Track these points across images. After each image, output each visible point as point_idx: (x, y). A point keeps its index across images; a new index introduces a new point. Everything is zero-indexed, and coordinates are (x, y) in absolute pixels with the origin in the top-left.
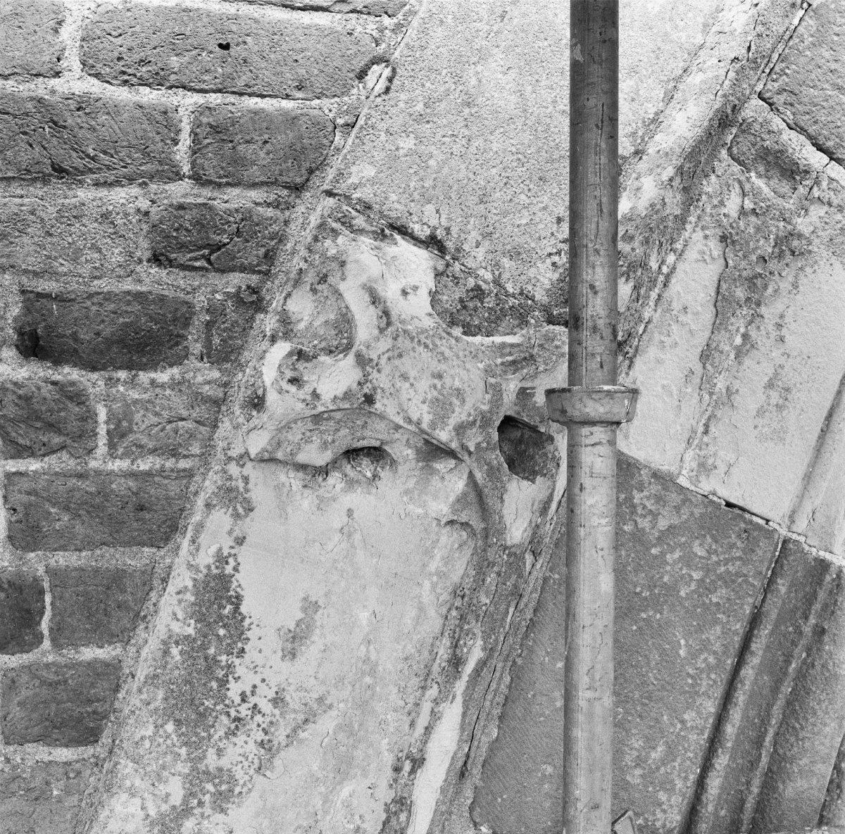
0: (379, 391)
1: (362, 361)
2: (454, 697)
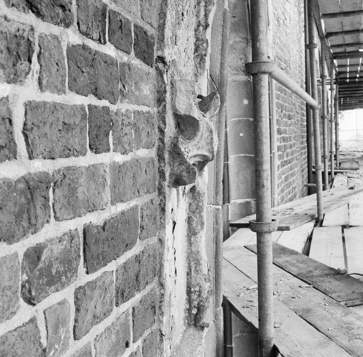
2: (214, 4)
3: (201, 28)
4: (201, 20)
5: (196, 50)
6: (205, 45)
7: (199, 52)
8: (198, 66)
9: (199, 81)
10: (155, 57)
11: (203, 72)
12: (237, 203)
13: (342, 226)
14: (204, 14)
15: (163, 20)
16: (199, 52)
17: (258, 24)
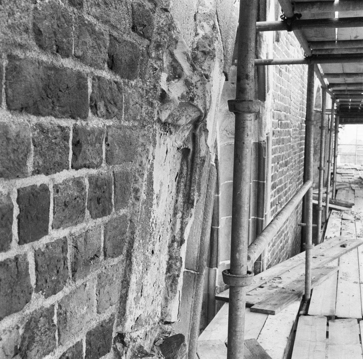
0: (197, 96)
1: (187, 83)
2: (191, 215)
3: (176, 244)
4: (175, 235)
5: (169, 269)
6: (178, 264)
7: (171, 273)
8: (169, 289)
9: (169, 307)
10: (114, 335)
11: (175, 296)
12: (226, 264)
13: (327, 317)
14: (180, 227)
15: (125, 289)
16: (171, 273)
17: (239, 234)
